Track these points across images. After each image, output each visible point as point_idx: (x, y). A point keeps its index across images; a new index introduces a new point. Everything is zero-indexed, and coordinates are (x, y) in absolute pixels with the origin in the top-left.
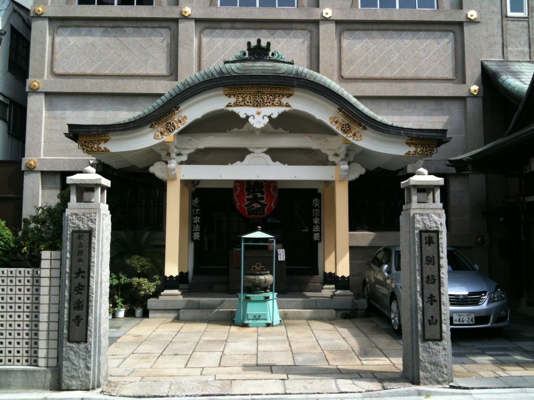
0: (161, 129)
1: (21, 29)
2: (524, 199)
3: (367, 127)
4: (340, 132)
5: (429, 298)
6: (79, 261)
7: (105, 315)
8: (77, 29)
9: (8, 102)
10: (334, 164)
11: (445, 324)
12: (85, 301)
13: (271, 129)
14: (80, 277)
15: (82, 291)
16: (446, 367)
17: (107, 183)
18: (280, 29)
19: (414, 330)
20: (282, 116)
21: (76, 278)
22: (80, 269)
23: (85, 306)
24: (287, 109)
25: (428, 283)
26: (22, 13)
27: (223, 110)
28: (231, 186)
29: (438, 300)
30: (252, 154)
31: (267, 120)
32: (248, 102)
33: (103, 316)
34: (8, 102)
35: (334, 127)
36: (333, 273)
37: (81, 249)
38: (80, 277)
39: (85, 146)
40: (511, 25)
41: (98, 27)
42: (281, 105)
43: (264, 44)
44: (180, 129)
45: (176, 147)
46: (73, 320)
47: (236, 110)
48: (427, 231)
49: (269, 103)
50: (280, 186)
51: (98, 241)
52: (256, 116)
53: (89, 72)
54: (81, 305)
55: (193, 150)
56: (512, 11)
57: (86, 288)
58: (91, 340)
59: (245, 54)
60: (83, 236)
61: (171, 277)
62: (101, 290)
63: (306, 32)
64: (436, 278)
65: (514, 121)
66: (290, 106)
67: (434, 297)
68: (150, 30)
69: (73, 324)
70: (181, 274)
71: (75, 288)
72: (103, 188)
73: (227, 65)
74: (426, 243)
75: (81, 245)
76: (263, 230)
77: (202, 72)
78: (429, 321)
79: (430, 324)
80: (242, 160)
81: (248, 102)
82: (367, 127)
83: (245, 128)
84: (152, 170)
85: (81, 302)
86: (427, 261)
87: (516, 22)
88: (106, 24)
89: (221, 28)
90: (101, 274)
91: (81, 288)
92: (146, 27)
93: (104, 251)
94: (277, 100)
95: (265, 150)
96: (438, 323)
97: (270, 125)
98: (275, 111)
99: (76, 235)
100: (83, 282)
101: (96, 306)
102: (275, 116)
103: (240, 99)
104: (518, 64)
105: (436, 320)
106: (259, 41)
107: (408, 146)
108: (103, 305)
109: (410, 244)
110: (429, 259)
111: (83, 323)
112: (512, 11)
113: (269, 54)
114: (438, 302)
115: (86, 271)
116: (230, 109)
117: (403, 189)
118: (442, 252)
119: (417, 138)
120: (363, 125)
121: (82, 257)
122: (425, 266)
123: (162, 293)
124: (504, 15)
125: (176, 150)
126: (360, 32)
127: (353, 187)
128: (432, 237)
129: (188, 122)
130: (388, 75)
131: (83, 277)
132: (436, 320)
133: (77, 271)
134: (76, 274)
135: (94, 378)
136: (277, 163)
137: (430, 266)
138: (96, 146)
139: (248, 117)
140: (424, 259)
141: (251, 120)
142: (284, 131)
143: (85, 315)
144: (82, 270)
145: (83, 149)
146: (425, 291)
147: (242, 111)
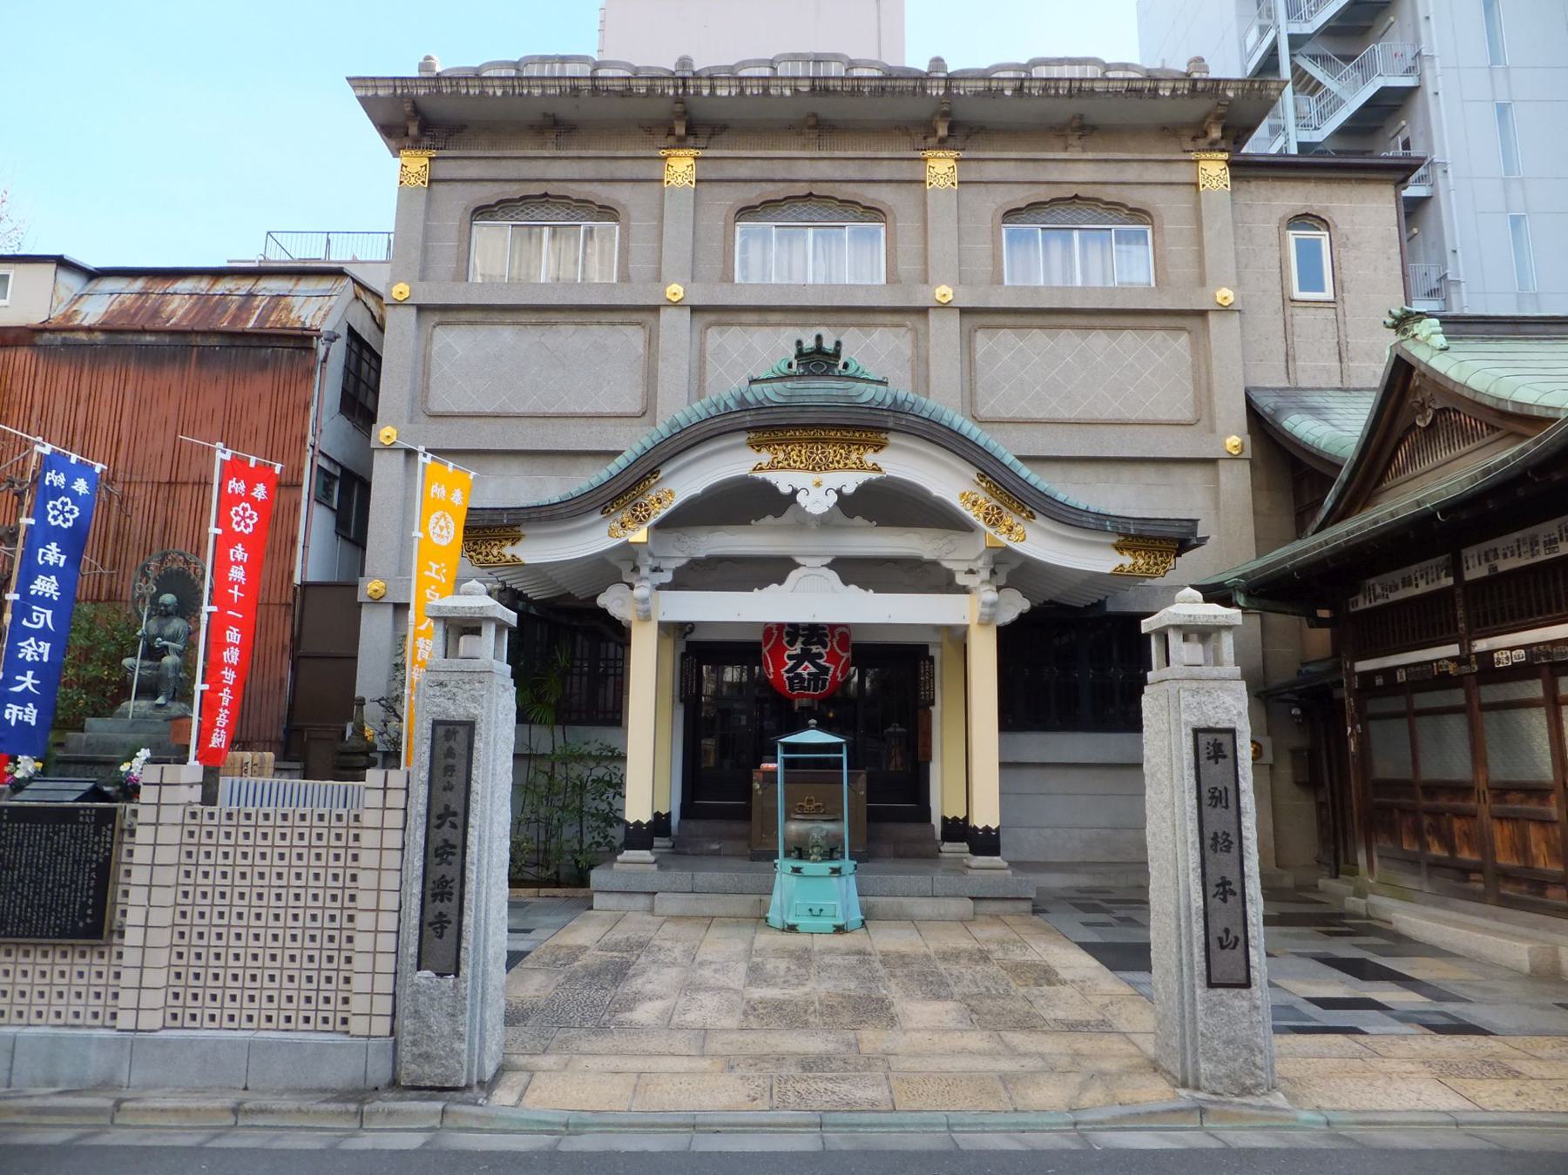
0: (624, 516)
1: (366, 331)
2: (1352, 666)
3: (1035, 513)
4: (981, 523)
5: (1218, 886)
6: (445, 789)
7: (499, 913)
8: (471, 327)
9: (338, 472)
10: (964, 590)
11: (1255, 947)
12: (457, 880)
13: (841, 518)
14: (448, 824)
15: (450, 857)
16: (1261, 1052)
17: (511, 617)
18: (852, 325)
19: (1184, 962)
20: (864, 490)
21: (439, 827)
22: (447, 807)
23: (456, 892)
24: (875, 476)
25: (1216, 851)
26: (371, 303)
27: (744, 479)
28: (758, 637)
29: (1238, 891)
30: (801, 569)
31: (834, 498)
32: (795, 462)
33: (493, 915)
34: (338, 472)
35: (970, 514)
36: (961, 817)
37: (450, 761)
38: (448, 824)
39: (475, 551)
40: (1302, 317)
41: (509, 324)
42: (861, 467)
43: (828, 345)
44: (659, 516)
45: (651, 555)
46: (431, 924)
47: (775, 478)
48: (1209, 730)
49: (838, 462)
50: (856, 638)
51: (487, 744)
52: (813, 490)
53: (488, 410)
54: (447, 889)
55: (684, 561)
56: (1301, 289)
57: (459, 851)
58: (466, 970)
59: (790, 366)
60: (455, 733)
61: (638, 823)
62: (490, 855)
63: (903, 330)
64: (1233, 838)
65: (1328, 503)
66: (880, 470)
67: (1230, 883)
68: (606, 328)
69: (429, 931)
70: (657, 815)
71: (436, 850)
72: (501, 626)
73: (755, 387)
74: (1209, 758)
75: (450, 753)
76: (819, 727)
77: (706, 401)
78: (1220, 939)
79: (1223, 947)
80: (781, 581)
81: (795, 462)
82: (1035, 513)
83: (788, 517)
84: (602, 601)
85: (447, 882)
86: (1212, 798)
87: (1312, 311)
88: (524, 318)
89: (740, 324)
90: (492, 819)
91: (448, 849)
92: (599, 323)
93: (498, 769)
94: (854, 456)
95: (829, 560)
96: (1240, 947)
97: (838, 510)
98: (850, 481)
99: (441, 730)
100: (454, 837)
101: (478, 893)
102: (849, 489)
103: (781, 456)
104: (1317, 393)
105: (1237, 939)
106: (819, 338)
107: (1117, 553)
108: (494, 891)
109: (1170, 759)
110: (1217, 794)
111: (450, 930)
112: (1301, 289)
113: (836, 366)
114: (1239, 897)
115: (460, 811)
116: (760, 475)
117: (1148, 636)
118: (1244, 779)
119: (1139, 537)
120: (1028, 508)
121: (453, 780)
122: (1206, 809)
123: (619, 858)
124: (1286, 297)
125: (650, 561)
126: (1009, 331)
127: (1009, 638)
128: (1220, 744)
129: (677, 501)
130: (1065, 414)
131: (454, 826)
132: (1237, 939)
133: (442, 811)
134: (439, 817)
135: (471, 1062)
136: (853, 587)
137: (1219, 810)
138: (495, 552)
139: (795, 492)
140: (1206, 795)
141: (800, 498)
142: (866, 522)
143: (456, 912)
144: (451, 809)
145: (471, 557)
146: (1208, 870)
147: (783, 481)
